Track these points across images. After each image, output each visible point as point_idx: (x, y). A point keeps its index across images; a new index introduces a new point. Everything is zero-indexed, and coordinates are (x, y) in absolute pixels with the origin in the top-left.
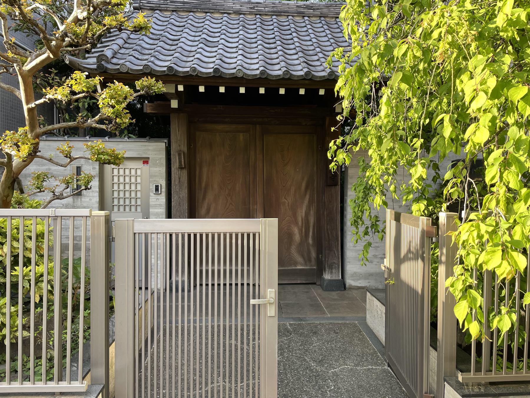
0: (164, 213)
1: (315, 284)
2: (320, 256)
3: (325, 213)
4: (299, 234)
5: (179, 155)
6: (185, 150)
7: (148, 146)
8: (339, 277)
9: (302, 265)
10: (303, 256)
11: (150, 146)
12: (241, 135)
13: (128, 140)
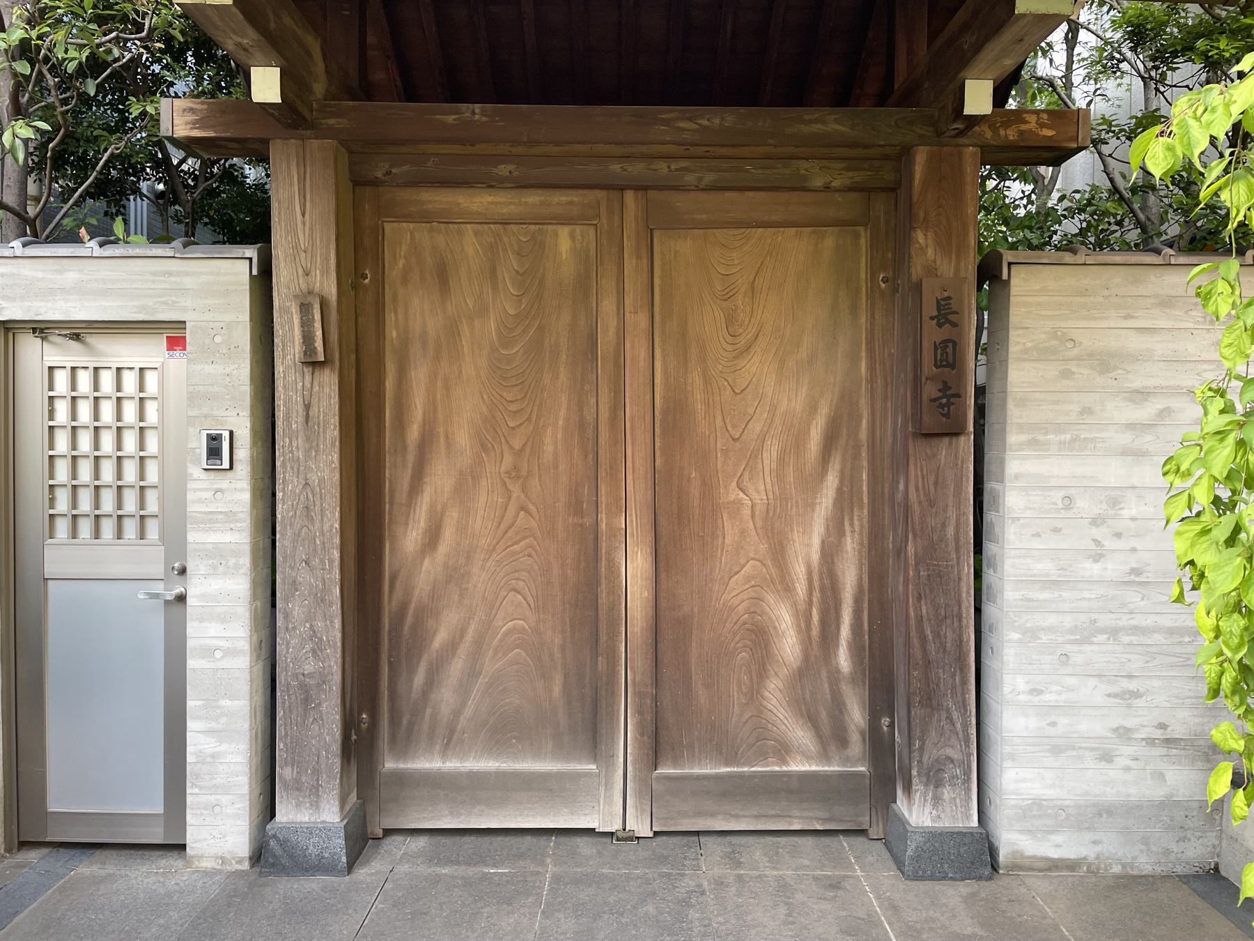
0: (247, 549)
1: (862, 832)
2: (885, 721)
3: (911, 548)
4: (799, 631)
5: (305, 308)
6: (331, 291)
7: (178, 274)
8: (968, 817)
9: (808, 758)
10: (812, 720)
11: (187, 274)
12: (564, 231)
13: (98, 251)
